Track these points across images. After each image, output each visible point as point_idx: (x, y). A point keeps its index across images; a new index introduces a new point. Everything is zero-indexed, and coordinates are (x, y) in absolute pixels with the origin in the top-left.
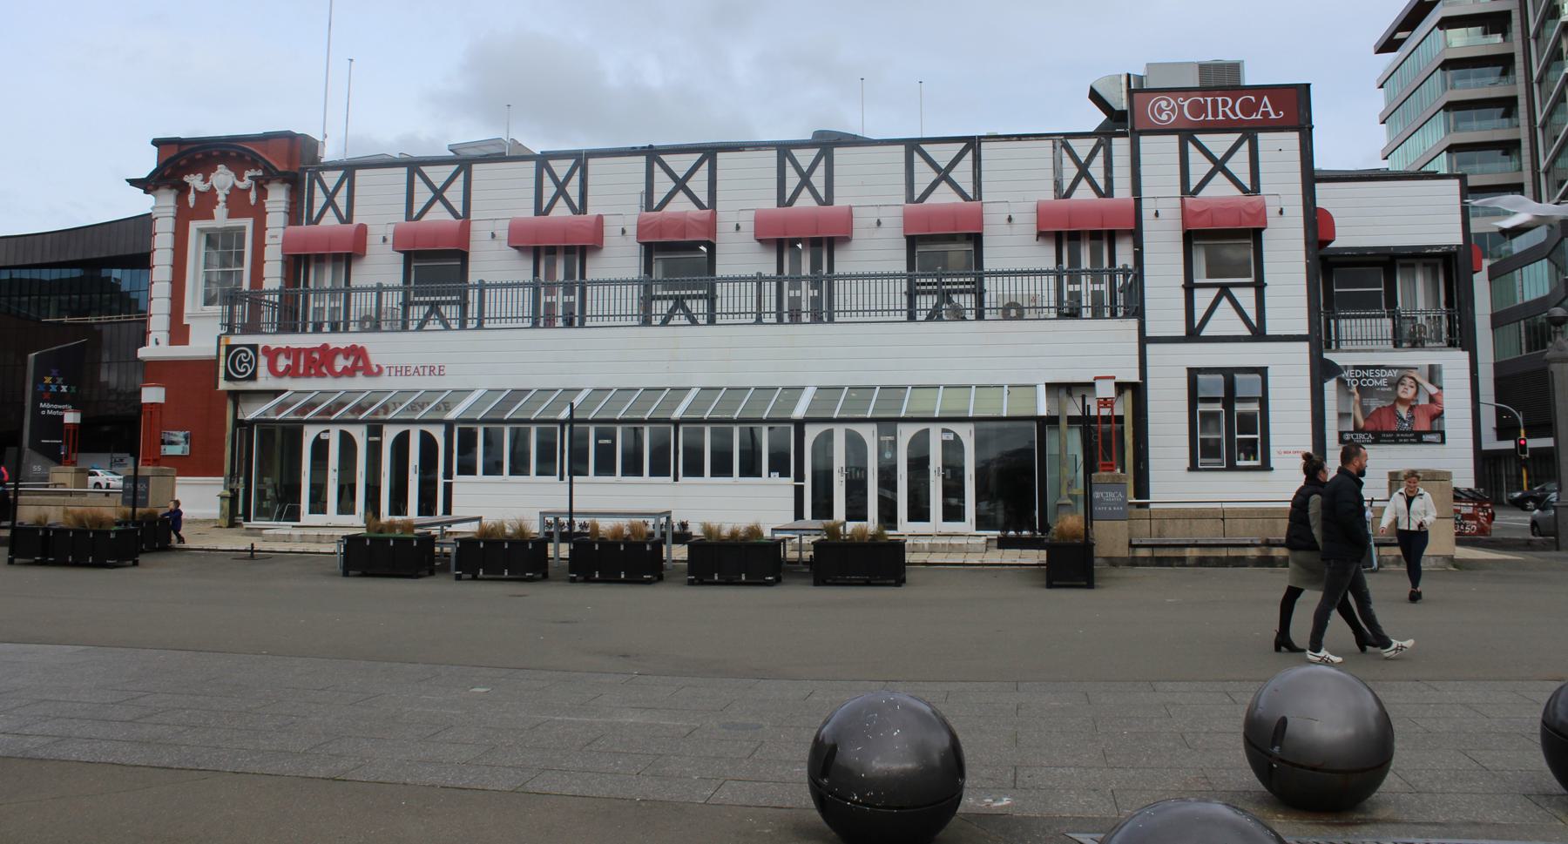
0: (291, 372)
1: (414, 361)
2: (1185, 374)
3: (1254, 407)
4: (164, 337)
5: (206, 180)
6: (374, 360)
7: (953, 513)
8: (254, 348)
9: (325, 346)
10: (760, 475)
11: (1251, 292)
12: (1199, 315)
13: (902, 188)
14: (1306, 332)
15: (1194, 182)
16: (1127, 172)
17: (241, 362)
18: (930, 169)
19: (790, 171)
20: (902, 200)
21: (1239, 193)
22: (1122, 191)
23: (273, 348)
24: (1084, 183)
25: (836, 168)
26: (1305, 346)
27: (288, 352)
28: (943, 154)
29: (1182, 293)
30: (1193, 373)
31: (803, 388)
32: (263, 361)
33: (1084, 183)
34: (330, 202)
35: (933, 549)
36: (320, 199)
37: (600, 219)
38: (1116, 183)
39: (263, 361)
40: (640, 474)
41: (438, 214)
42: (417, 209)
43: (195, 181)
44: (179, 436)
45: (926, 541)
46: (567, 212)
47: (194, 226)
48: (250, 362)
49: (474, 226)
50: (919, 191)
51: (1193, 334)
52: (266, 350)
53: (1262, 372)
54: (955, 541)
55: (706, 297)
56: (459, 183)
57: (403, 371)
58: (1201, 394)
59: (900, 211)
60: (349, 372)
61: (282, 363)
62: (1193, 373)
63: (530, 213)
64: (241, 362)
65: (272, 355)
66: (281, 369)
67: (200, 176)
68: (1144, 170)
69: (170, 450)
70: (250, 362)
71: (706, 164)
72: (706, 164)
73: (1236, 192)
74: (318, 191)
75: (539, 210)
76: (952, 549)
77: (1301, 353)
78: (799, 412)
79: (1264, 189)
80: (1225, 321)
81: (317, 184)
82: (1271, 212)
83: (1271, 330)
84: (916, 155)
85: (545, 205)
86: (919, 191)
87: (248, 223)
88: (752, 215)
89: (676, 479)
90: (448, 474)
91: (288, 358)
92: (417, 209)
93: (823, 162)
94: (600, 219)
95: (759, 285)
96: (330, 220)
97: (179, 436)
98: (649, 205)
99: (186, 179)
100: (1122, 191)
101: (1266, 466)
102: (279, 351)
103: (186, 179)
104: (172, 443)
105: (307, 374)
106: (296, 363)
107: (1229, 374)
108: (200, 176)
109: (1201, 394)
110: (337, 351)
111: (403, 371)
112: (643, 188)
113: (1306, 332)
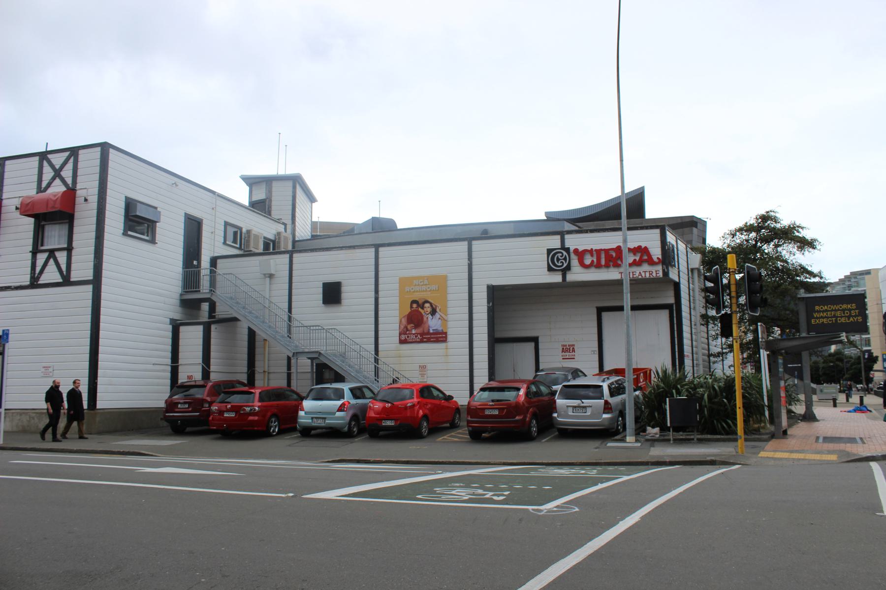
11: (65, 253)
17: (558, 260)
23: (581, 249)
28: (57, 160)
32: (575, 262)
38: (485, 350)
39: (575, 262)
48: (565, 259)
61: (588, 260)
63: (35, 192)
64: (558, 260)
65: (581, 254)
70: (565, 259)
71: (72, 158)
75: (40, 190)
76: (424, 470)
91: (592, 255)
92: (44, 184)
93: (72, 160)
105: (607, 266)
106: (599, 258)
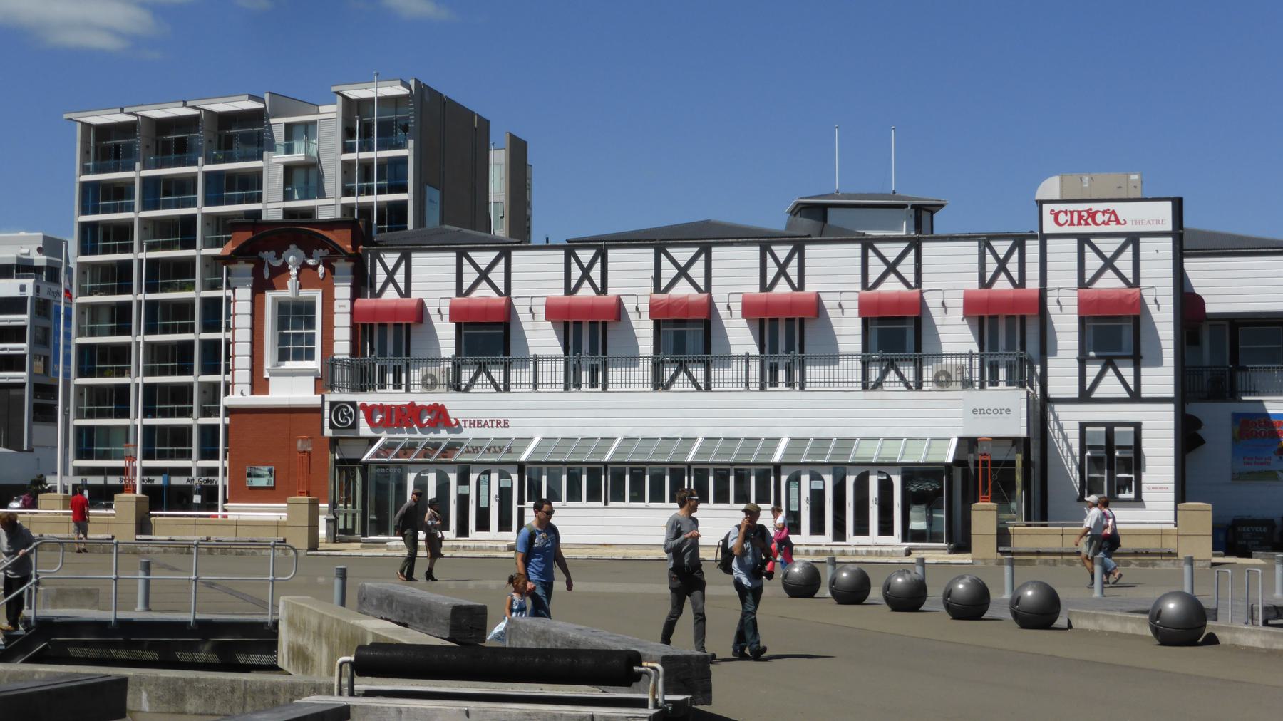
0: (386, 424)
1: (484, 415)
2: (1077, 426)
3: (1130, 454)
4: (247, 388)
5: (278, 257)
6: (453, 414)
7: (886, 529)
8: (353, 404)
9: (412, 404)
10: (581, 500)
12: (1089, 381)
13: (859, 278)
14: (1172, 395)
15: (1089, 275)
16: (1037, 266)
18: (880, 262)
19: (770, 262)
20: (858, 287)
21: (1123, 285)
22: (1033, 283)
24: (1003, 276)
25: (806, 260)
26: (1171, 407)
27: (382, 408)
29: (1076, 363)
30: (1083, 426)
31: (779, 439)
33: (1003, 276)
34: (391, 278)
35: (869, 553)
36: (381, 277)
37: (619, 298)
38: (1028, 275)
40: (727, 501)
41: (484, 292)
42: (466, 286)
43: (269, 256)
44: (264, 470)
45: (864, 549)
46: (592, 293)
47: (269, 296)
49: (515, 302)
50: (872, 279)
51: (1085, 396)
52: (363, 406)
53: (1137, 426)
54: (883, 549)
55: (602, 255)
56: (501, 266)
57: (477, 423)
58: (1088, 444)
59: (856, 296)
60: (434, 425)
62: (1083, 426)
66: (377, 421)
67: (273, 253)
68: (1050, 265)
69: (257, 482)
71: (703, 256)
72: (703, 256)
73: (1121, 284)
74: (379, 269)
76: (881, 554)
77: (1169, 411)
78: (777, 458)
79: (1143, 283)
80: (1110, 386)
81: (378, 263)
82: (1149, 300)
83: (1145, 393)
84: (870, 252)
85: (573, 285)
86: (872, 279)
87: (318, 296)
88: (740, 298)
89: (606, 503)
90: (521, 501)
94: (619, 298)
95: (747, 362)
96: (390, 295)
97: (264, 470)
98: (657, 288)
99: (261, 254)
100: (1033, 283)
101: (1138, 499)
102: (374, 407)
103: (261, 254)
104: (258, 476)
107: (1110, 427)
108: (273, 253)
109: (1088, 444)
110: (422, 407)
111: (477, 423)
112: (652, 273)
113: (1172, 395)
